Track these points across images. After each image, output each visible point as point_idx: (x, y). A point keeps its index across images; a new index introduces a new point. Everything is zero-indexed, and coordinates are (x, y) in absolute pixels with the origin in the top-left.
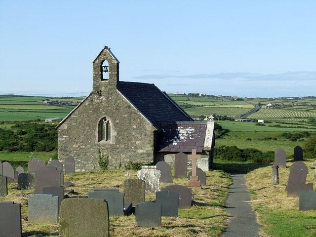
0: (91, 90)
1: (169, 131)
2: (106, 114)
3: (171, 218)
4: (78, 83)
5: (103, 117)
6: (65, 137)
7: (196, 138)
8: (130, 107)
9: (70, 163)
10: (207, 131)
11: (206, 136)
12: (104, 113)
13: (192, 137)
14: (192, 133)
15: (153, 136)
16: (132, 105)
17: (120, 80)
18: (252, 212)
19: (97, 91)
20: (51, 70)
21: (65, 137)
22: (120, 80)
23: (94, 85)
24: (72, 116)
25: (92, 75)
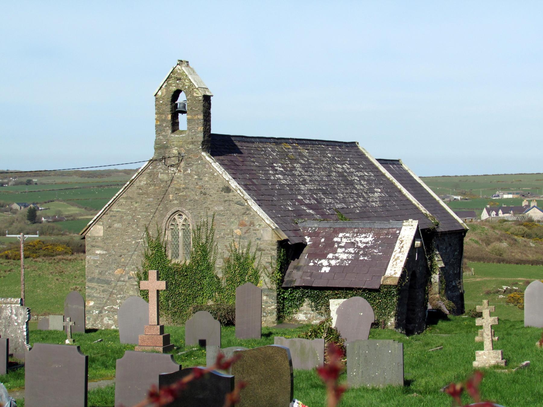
0: (151, 154)
1: (320, 243)
2: (181, 204)
3: (364, 235)
4: (120, 134)
5: (173, 210)
6: (98, 252)
7: (374, 257)
8: (228, 189)
9: (74, 306)
10: (398, 242)
11: (394, 254)
12: (175, 202)
13: (364, 255)
14: (366, 247)
15: (275, 253)
16: (233, 184)
17: (214, 130)
18: (395, 316)
19: (161, 156)
20: (90, 119)
21: (98, 252)
22: (214, 130)
23: (156, 144)
24: (115, 208)
25: (154, 123)
